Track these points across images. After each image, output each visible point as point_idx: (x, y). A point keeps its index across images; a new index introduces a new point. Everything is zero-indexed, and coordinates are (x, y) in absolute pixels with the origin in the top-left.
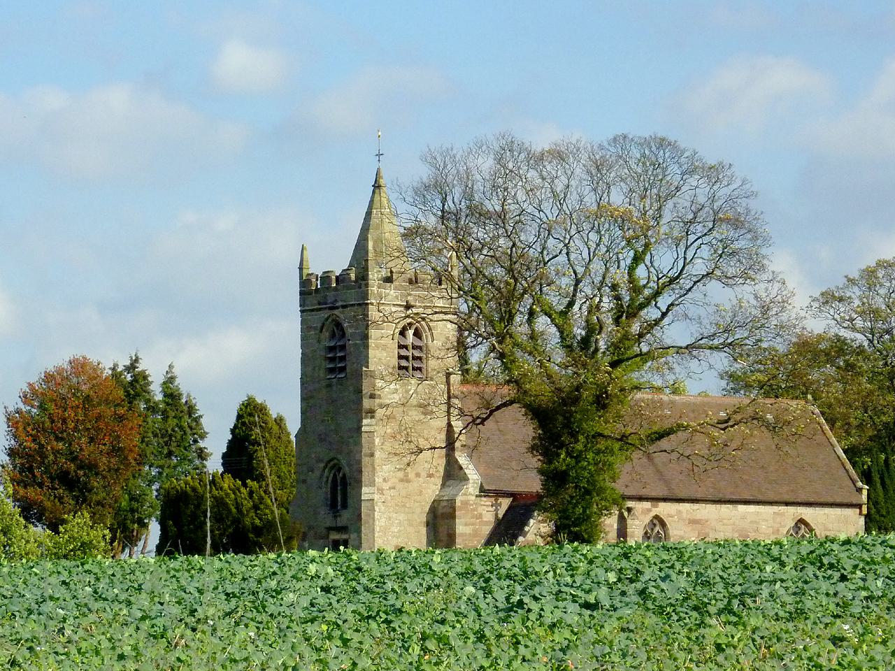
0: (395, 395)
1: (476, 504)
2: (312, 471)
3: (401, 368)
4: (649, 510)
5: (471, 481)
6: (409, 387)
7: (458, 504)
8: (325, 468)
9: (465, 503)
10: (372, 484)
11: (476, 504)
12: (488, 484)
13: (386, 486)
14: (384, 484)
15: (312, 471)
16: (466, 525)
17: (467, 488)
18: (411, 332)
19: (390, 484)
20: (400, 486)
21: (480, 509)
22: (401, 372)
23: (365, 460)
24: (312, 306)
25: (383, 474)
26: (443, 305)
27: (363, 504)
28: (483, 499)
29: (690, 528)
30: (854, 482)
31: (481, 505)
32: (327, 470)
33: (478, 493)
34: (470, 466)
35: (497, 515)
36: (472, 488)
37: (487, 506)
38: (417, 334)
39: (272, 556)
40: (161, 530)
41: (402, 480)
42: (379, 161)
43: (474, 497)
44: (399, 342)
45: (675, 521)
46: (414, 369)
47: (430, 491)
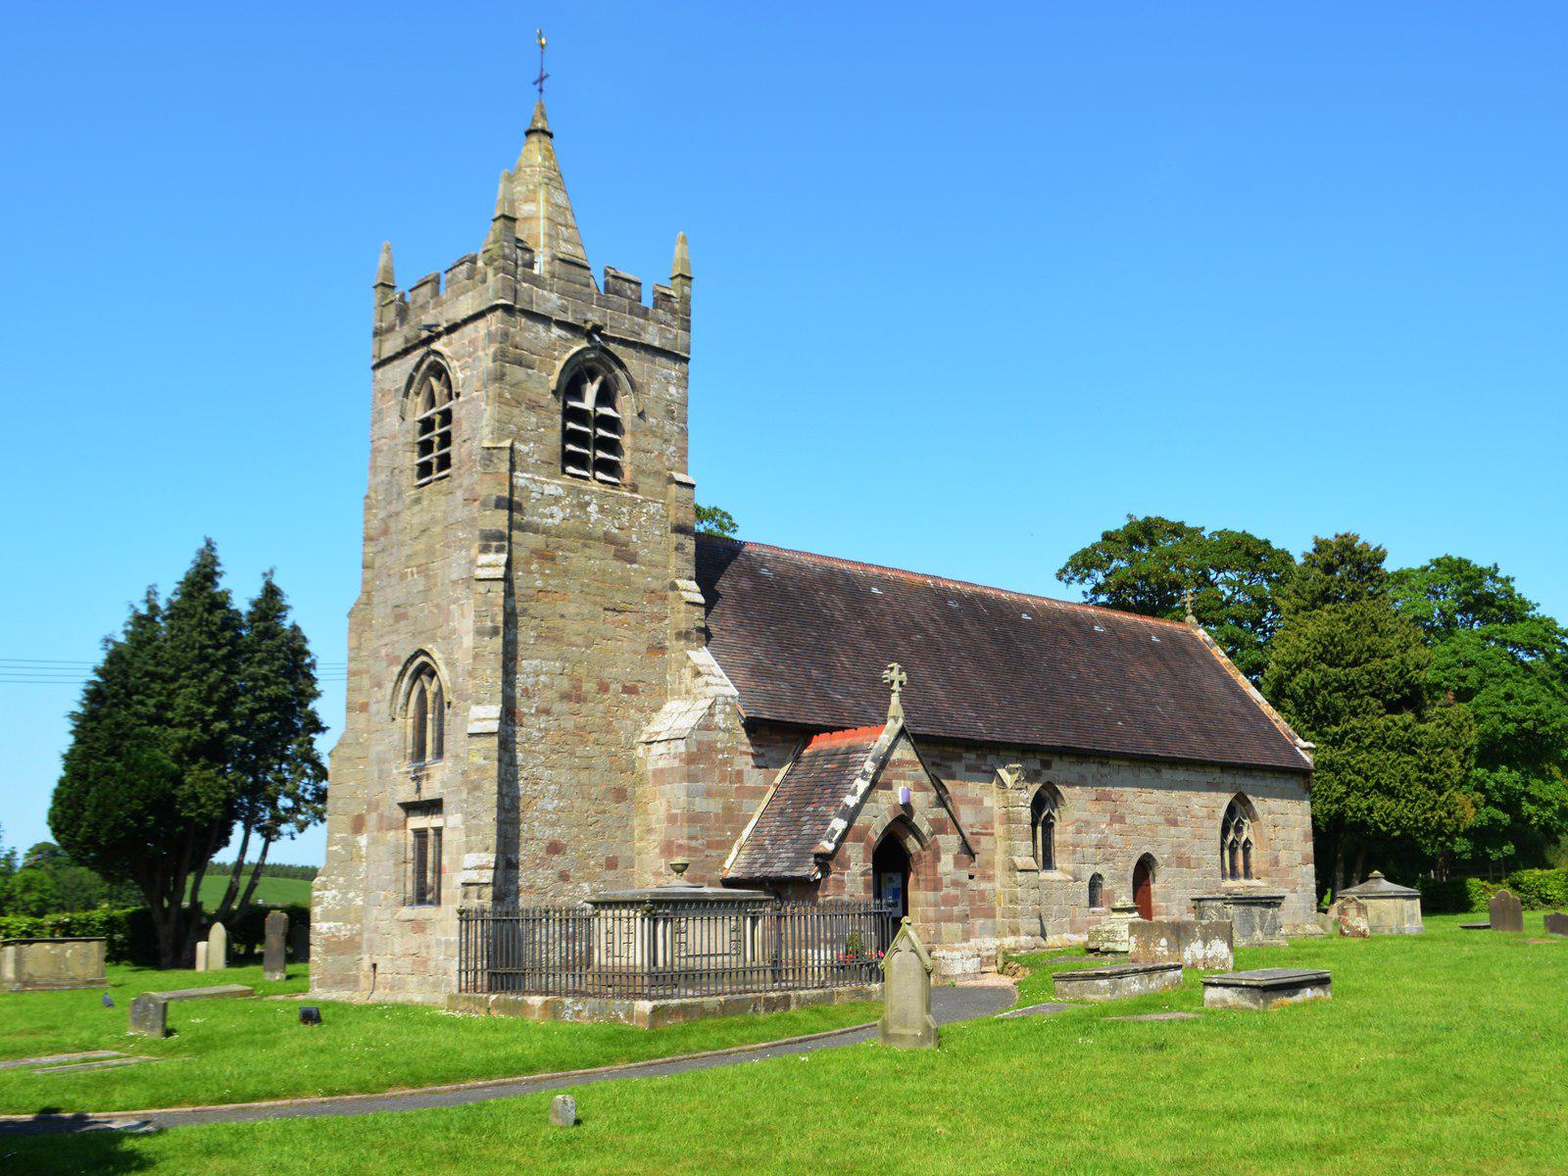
2: (379, 685)
8: (402, 674)
15: (379, 685)
20: (560, 707)
32: (406, 679)
39: (521, 782)
40: (69, 759)
41: (565, 697)
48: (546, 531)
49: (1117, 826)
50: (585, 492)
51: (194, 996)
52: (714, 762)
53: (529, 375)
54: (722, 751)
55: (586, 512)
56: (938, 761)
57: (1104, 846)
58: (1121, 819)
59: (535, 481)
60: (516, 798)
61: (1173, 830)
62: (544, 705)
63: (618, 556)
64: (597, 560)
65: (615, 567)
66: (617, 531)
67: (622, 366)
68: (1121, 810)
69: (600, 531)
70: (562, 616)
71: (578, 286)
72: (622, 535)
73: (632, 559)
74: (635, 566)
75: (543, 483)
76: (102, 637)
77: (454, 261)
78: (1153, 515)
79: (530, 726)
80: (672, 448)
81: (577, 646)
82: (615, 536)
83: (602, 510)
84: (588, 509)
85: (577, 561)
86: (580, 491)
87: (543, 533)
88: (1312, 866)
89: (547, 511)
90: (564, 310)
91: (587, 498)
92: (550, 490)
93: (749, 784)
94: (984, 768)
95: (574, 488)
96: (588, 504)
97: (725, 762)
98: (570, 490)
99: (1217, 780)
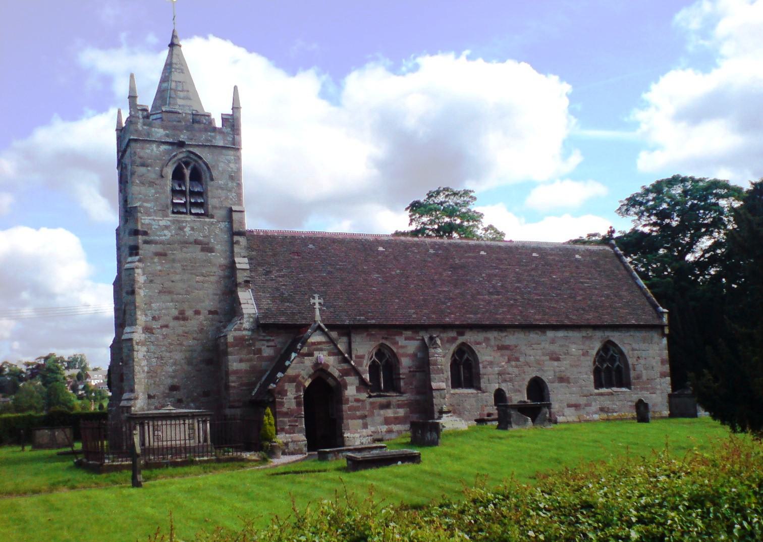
0: (166, 232)
4: (454, 339)
5: (245, 316)
11: (252, 339)
16: (241, 361)
20: (172, 324)
24: (17, 411)
29: (499, 354)
30: (655, 307)
34: (250, 301)
45: (483, 348)
48: (162, 243)
49: (513, 363)
50: (183, 222)
53: (148, 170)
55: (184, 232)
56: (386, 336)
57: (504, 374)
58: (517, 359)
59: (154, 220)
61: (556, 363)
62: (165, 323)
63: (203, 250)
64: (196, 253)
65: (201, 255)
66: (202, 238)
67: (200, 158)
68: (517, 355)
69: (192, 239)
70: (173, 281)
71: (175, 123)
72: (205, 240)
74: (213, 254)
75: (158, 220)
77: (242, 103)
78: (676, 174)
81: (182, 295)
84: (185, 230)
85: (179, 255)
86: (179, 221)
87: (160, 243)
88: (668, 379)
89: (162, 233)
90: (167, 136)
91: (184, 224)
92: (162, 223)
93: (265, 355)
94: (417, 338)
96: (185, 227)
98: (173, 222)
99: (590, 335)
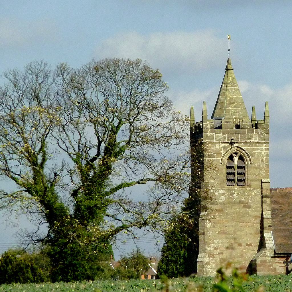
1: (272, 262)
3: (228, 180)
5: (267, 248)
6: (233, 192)
7: (258, 262)
9: (264, 262)
10: (204, 251)
12: (279, 249)
13: (216, 252)
14: (215, 251)
17: (264, 252)
18: (236, 159)
19: (219, 251)
21: (275, 266)
22: (230, 183)
23: (201, 237)
25: (214, 245)
26: (258, 141)
27: (198, 264)
28: (277, 259)
31: (276, 263)
33: (273, 255)
35: (287, 268)
36: (268, 252)
37: (280, 263)
38: (241, 158)
41: (227, 248)
42: (229, 54)
43: (270, 258)
44: (227, 165)
46: (239, 180)
47: (249, 255)
51: (212, 142)
52: (266, 266)
54: (269, 263)
60: (261, 234)
65: (244, 210)
70: (226, 227)
72: (246, 201)
73: (249, 207)
76: (63, 61)
79: (216, 258)
80: (263, 171)
82: (243, 201)
83: (238, 194)
95: (229, 189)
96: (234, 193)
97: (269, 266)
